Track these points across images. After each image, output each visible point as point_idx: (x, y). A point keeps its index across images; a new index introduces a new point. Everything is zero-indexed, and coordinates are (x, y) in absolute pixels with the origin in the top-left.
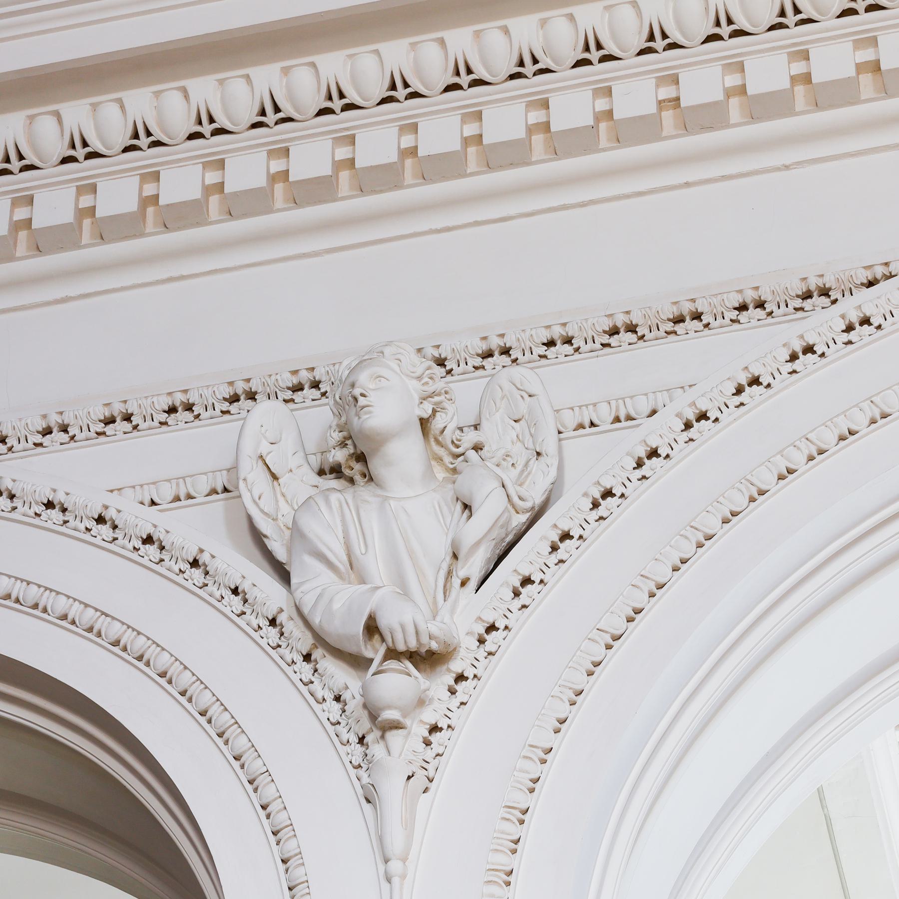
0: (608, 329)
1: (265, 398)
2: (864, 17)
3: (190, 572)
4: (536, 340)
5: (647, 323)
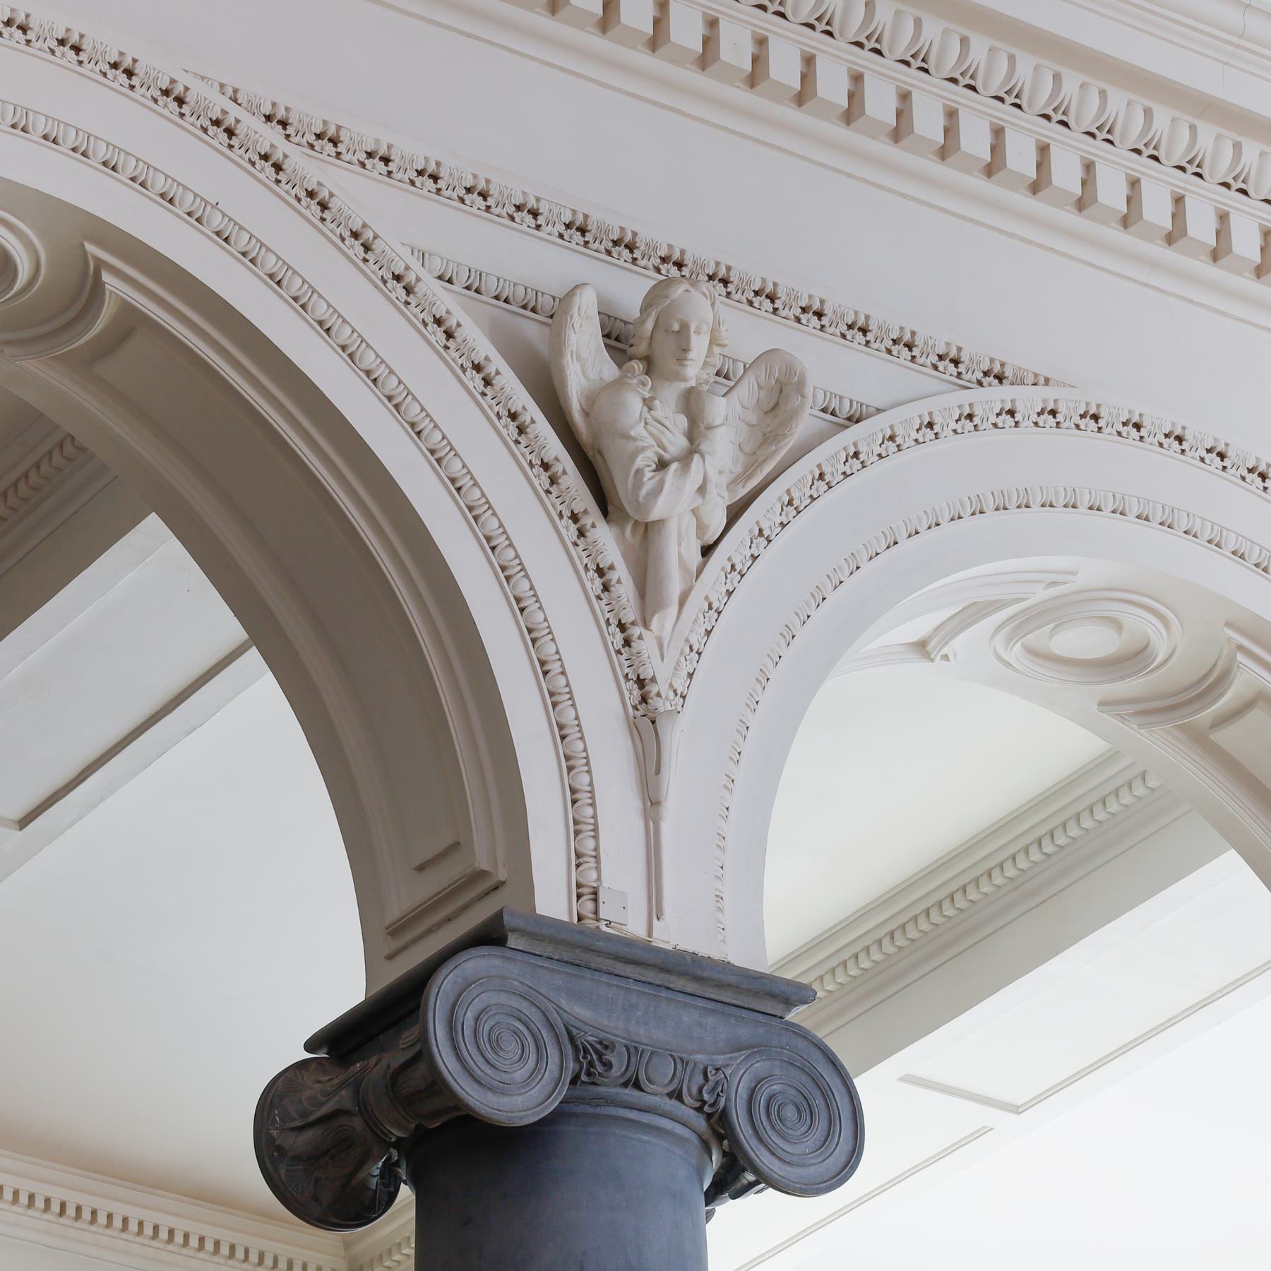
2: (1007, 108)
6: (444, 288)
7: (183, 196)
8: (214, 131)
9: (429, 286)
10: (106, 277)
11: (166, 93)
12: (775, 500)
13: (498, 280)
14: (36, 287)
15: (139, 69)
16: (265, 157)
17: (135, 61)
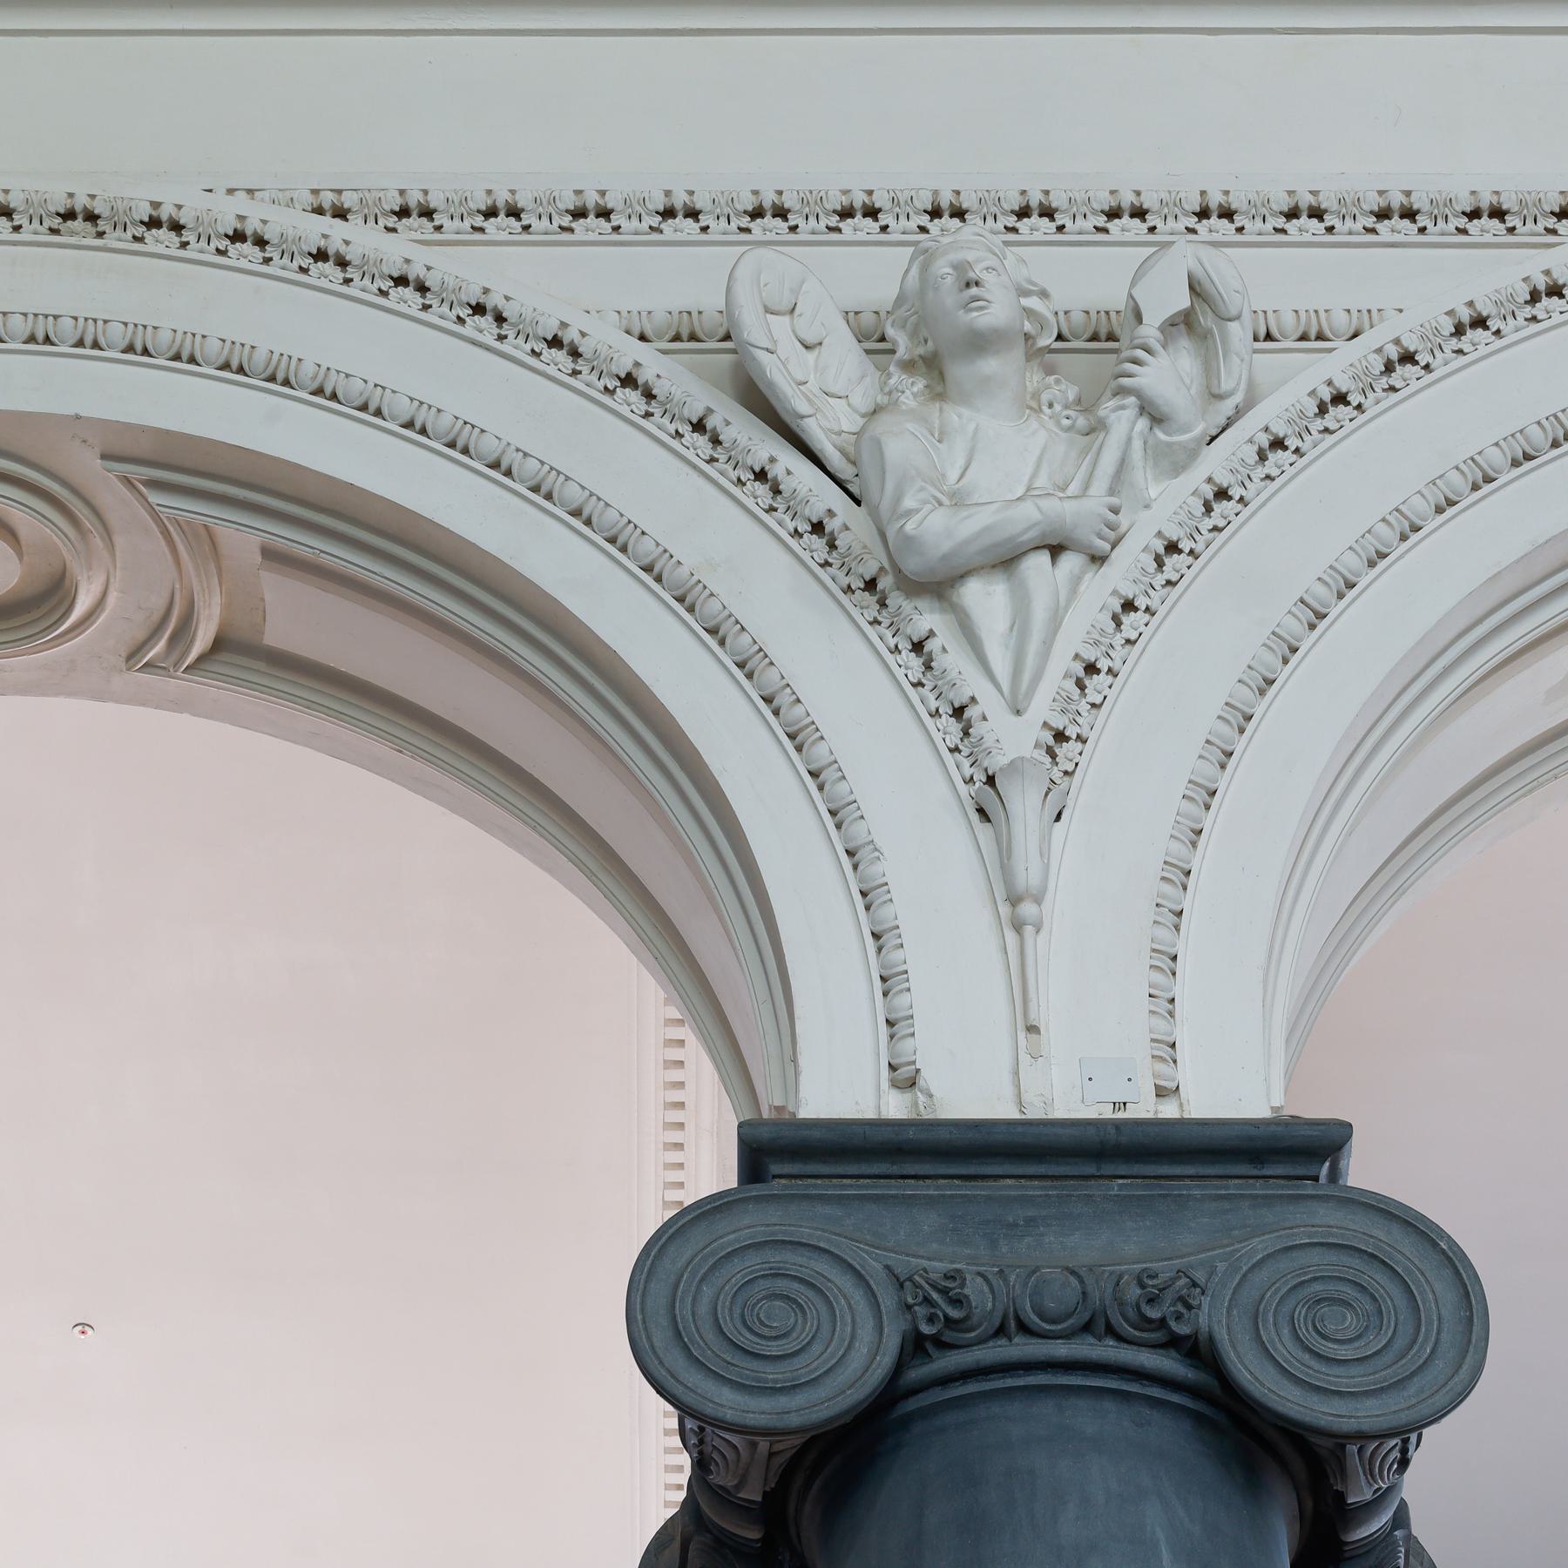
0: (572, 208)
1: (360, 221)
3: (754, 487)
4: (1364, 207)
5: (28, 211)
8: (1398, 379)
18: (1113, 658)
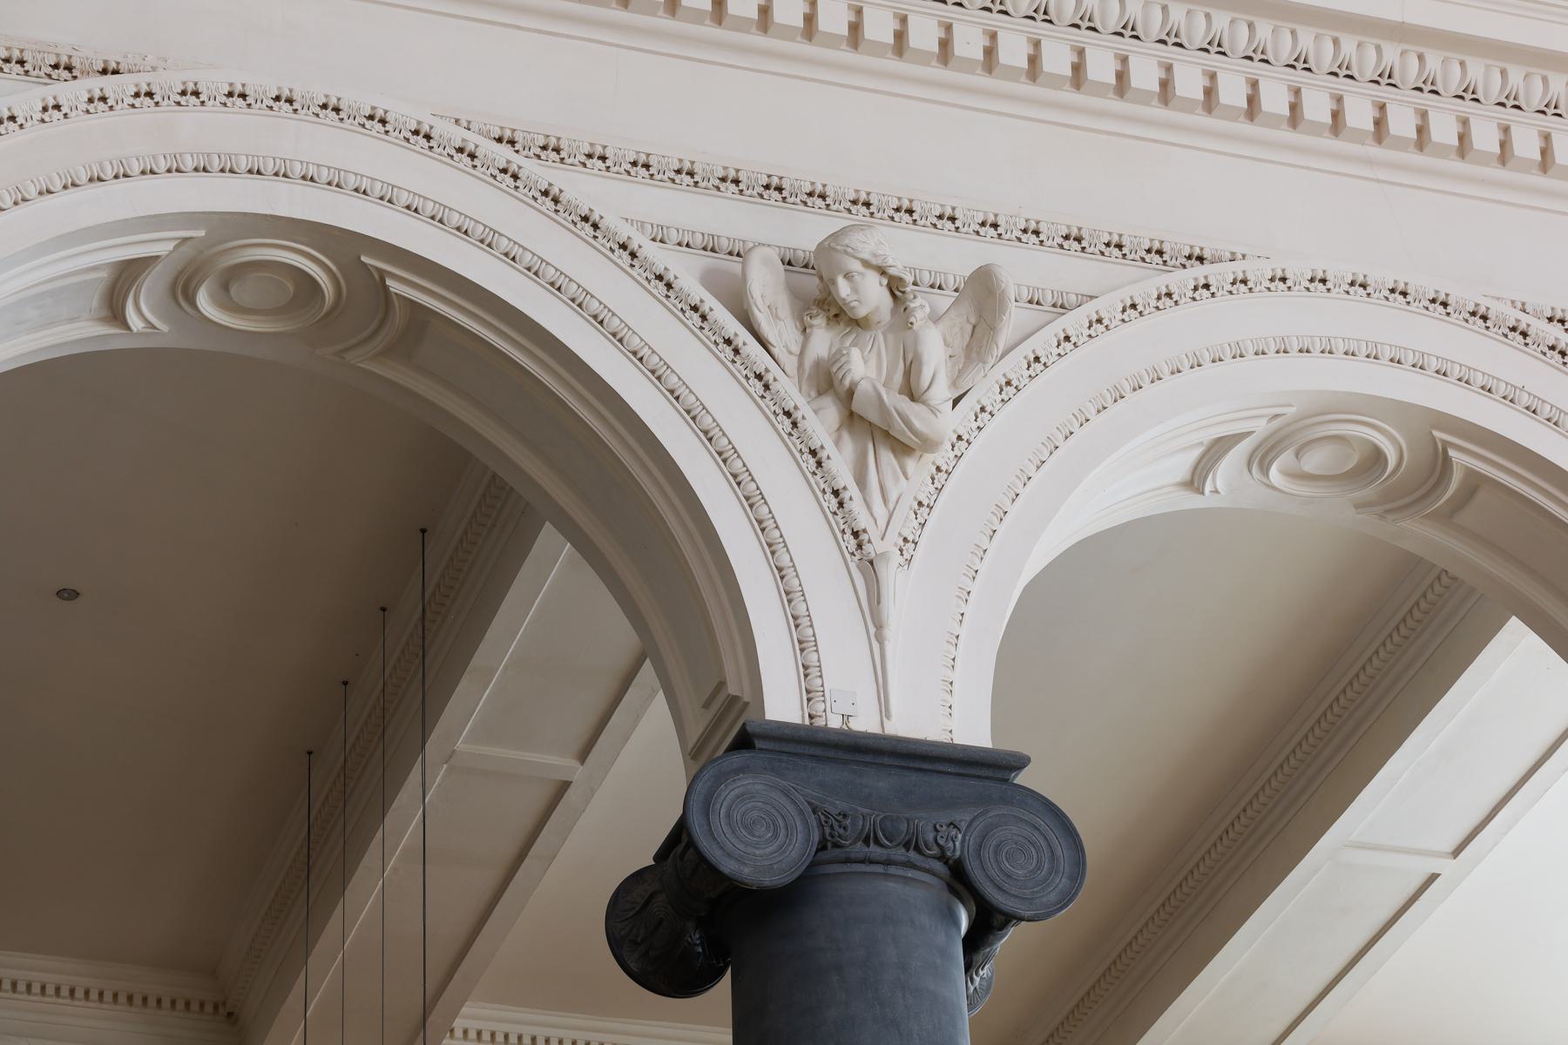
2: (1257, 64)
6: (660, 248)
7: (1497, 385)
9: (650, 250)
10: (1452, 453)
11: (1473, 314)
12: (994, 382)
13: (930, 272)
14: (1402, 470)
15: (1451, 301)
16: (1552, 348)
17: (1447, 295)
18: (909, 476)
